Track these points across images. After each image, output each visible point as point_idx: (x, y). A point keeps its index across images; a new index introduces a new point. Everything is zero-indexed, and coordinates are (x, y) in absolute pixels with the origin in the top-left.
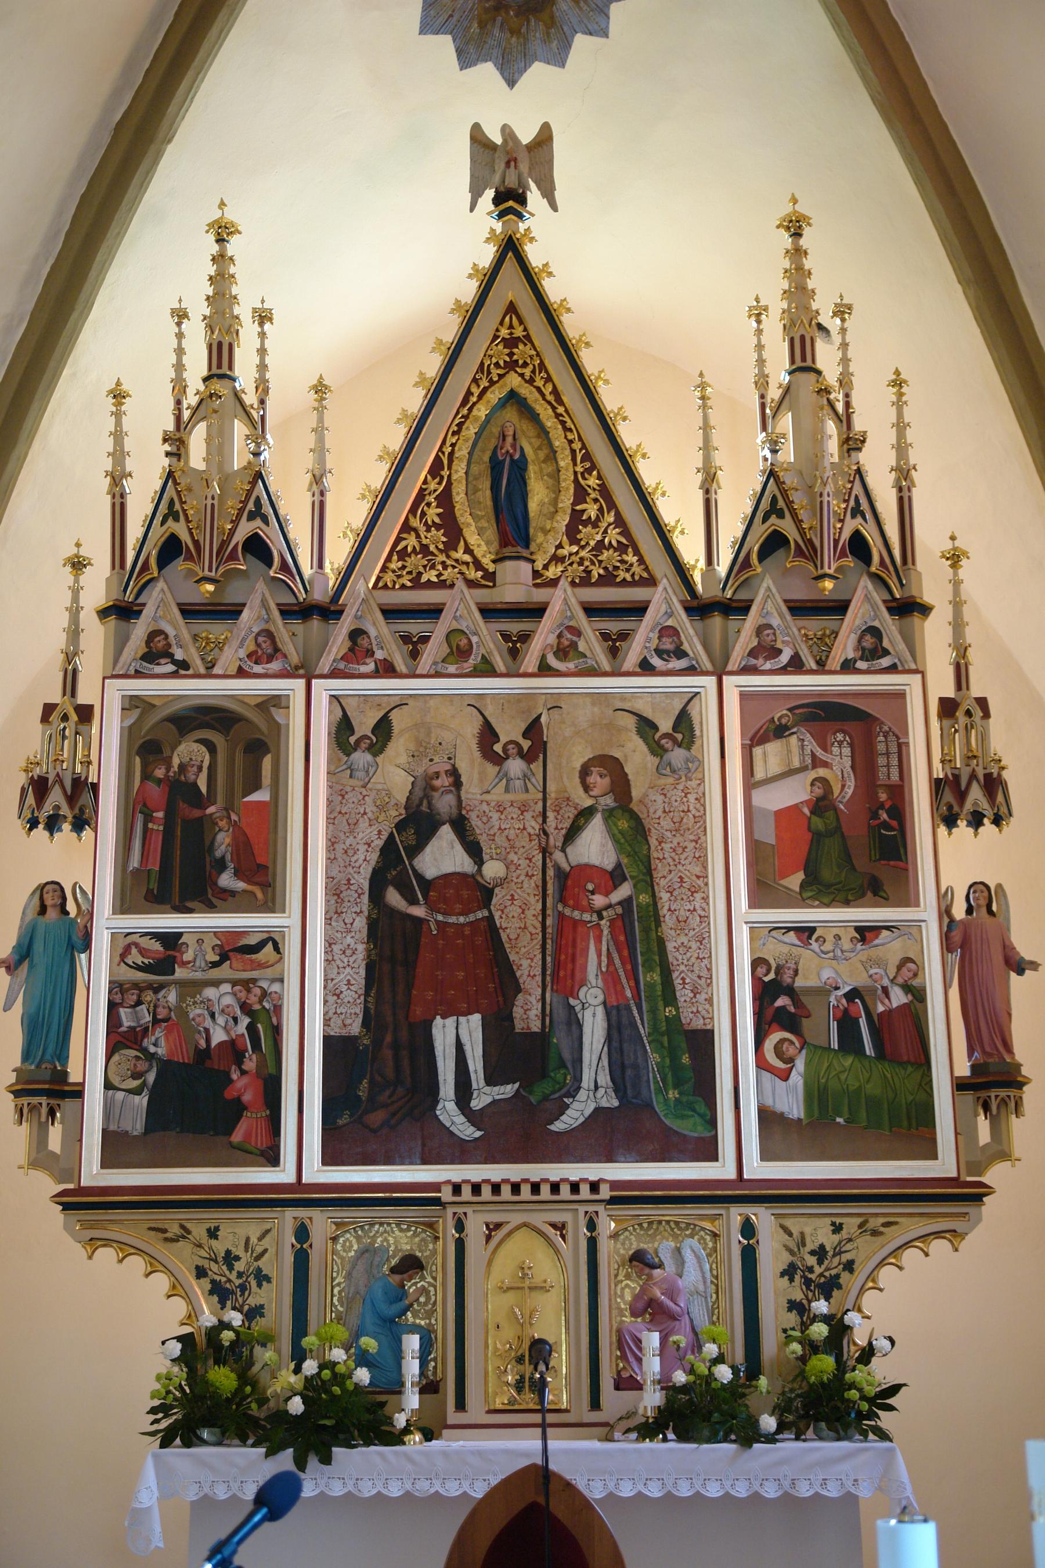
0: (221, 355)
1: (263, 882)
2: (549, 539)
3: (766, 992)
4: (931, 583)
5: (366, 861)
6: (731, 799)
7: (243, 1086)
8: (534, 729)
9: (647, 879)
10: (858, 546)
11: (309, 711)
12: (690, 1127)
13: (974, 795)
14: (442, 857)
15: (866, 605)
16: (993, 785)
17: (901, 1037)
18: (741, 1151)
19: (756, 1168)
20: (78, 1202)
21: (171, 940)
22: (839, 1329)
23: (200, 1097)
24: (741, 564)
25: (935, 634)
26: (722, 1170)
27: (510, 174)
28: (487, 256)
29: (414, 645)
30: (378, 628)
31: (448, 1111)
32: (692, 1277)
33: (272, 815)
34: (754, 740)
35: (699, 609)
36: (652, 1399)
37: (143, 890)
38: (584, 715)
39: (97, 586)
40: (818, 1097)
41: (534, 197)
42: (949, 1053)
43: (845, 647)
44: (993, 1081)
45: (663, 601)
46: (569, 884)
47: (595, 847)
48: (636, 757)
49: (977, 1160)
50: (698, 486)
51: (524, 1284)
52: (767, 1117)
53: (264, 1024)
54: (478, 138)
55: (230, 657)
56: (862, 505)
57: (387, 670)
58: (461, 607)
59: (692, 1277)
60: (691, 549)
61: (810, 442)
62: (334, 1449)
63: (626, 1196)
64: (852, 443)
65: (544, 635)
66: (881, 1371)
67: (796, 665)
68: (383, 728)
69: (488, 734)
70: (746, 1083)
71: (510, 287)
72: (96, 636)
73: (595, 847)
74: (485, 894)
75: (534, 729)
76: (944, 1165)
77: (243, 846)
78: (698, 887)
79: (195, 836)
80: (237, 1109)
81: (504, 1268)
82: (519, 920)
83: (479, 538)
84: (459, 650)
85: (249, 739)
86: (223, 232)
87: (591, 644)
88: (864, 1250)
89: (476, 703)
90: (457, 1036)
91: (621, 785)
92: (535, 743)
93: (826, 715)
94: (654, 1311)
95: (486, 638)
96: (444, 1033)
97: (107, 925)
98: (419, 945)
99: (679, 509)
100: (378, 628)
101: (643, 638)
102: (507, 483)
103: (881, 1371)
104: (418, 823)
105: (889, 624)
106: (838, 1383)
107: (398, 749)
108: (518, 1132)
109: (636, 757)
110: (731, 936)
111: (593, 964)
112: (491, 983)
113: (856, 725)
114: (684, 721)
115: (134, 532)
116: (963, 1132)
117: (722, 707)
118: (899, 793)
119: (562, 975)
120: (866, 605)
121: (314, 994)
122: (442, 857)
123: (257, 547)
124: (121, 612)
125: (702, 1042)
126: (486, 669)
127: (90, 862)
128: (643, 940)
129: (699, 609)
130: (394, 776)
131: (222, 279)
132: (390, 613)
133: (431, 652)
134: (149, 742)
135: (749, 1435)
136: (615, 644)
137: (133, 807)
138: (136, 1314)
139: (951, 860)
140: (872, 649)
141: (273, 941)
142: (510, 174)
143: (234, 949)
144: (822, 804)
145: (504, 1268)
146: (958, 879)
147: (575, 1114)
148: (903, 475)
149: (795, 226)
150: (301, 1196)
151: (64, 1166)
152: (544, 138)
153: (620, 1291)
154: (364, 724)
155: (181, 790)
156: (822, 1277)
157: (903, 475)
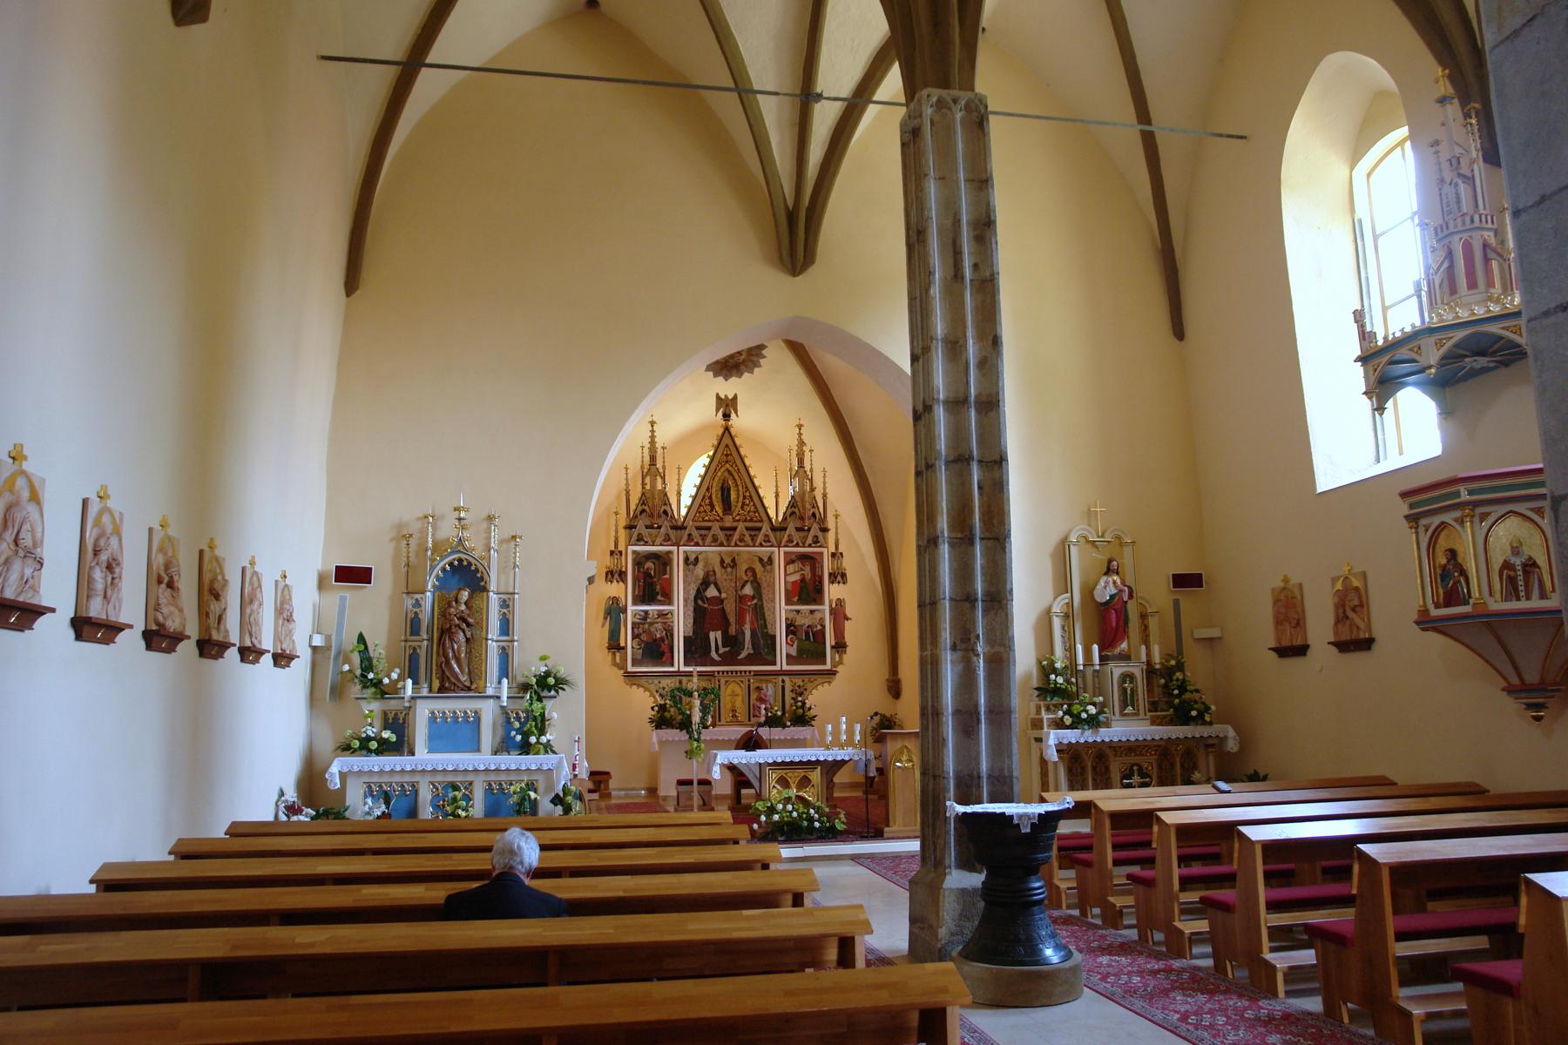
0: (653, 458)
1: (668, 598)
2: (737, 509)
3: (788, 626)
4: (831, 524)
5: (693, 593)
6: (781, 578)
7: (664, 647)
8: (733, 560)
9: (761, 599)
10: (814, 515)
11: (678, 554)
12: (769, 658)
13: (839, 576)
14: (712, 592)
15: (815, 530)
16: (843, 575)
17: (820, 636)
18: (782, 663)
19: (785, 667)
20: (630, 676)
21: (646, 612)
22: (804, 703)
23: (655, 649)
24: (785, 519)
25: (831, 536)
26: (777, 668)
27: (727, 406)
28: (721, 431)
29: (703, 537)
30: (695, 533)
31: (713, 654)
32: (770, 692)
33: (669, 582)
34: (787, 563)
35: (774, 529)
36: (763, 719)
37: (640, 599)
38: (746, 557)
39: (623, 522)
40: (799, 650)
41: (733, 415)
42: (830, 640)
43: (809, 540)
44: (840, 646)
45: (766, 528)
46: (742, 599)
47: (748, 590)
48: (758, 568)
49: (835, 664)
50: (775, 493)
51: (734, 694)
52: (788, 656)
53: (669, 632)
54: (718, 396)
55: (658, 541)
56: (815, 505)
57: (697, 544)
58: (716, 527)
59: (770, 692)
60: (772, 513)
61: (802, 485)
62: (1326, 480)
63: (757, 673)
64: (813, 489)
65: (736, 536)
66: (812, 713)
67: (797, 545)
68: (697, 559)
69: (722, 561)
70: (783, 647)
71: (727, 440)
72: (623, 534)
73: (748, 590)
74: (722, 601)
75: (733, 560)
76: (828, 666)
77: (662, 588)
78: (773, 600)
79: (652, 586)
80: (663, 654)
81: (729, 691)
82: (730, 608)
83: (719, 508)
84: (715, 539)
85: (663, 561)
86: (652, 423)
87: (747, 538)
88: (809, 686)
89: (720, 553)
90: (715, 636)
91: (754, 574)
92: (734, 564)
93: (804, 558)
94: (761, 700)
95: (721, 536)
96: (712, 635)
97: (631, 608)
98: (705, 614)
99: (769, 502)
100: (695, 533)
101: (760, 538)
102: (725, 491)
103: (812, 713)
104: (705, 583)
105: (820, 534)
106: (803, 715)
107: (700, 565)
108: (728, 659)
109: (758, 568)
110: (780, 612)
111: (748, 619)
112: (724, 625)
113: (812, 560)
114: (770, 560)
115: (633, 507)
116: (832, 658)
117: (779, 555)
118: (821, 577)
119: (740, 622)
120: (815, 530)
121: (681, 626)
122: (712, 592)
123: (665, 512)
124: (630, 527)
125: (774, 637)
126: (722, 545)
127: (624, 591)
128: (760, 613)
129: (774, 529)
130: (700, 571)
131: (653, 437)
132: (698, 528)
133: (709, 539)
134: (640, 560)
135: (784, 726)
136: (753, 538)
137: (635, 579)
138: (643, 702)
139: (832, 592)
140: (816, 541)
141: (671, 612)
142: (727, 406)
143: (661, 615)
144: (803, 580)
145: (729, 691)
146: (834, 597)
147: (742, 656)
148: (825, 495)
149: (800, 427)
150: (782, 673)
151: (622, 666)
152: (735, 397)
153: (754, 696)
154: (692, 558)
155: (647, 574)
156: (799, 692)
157: (825, 495)
